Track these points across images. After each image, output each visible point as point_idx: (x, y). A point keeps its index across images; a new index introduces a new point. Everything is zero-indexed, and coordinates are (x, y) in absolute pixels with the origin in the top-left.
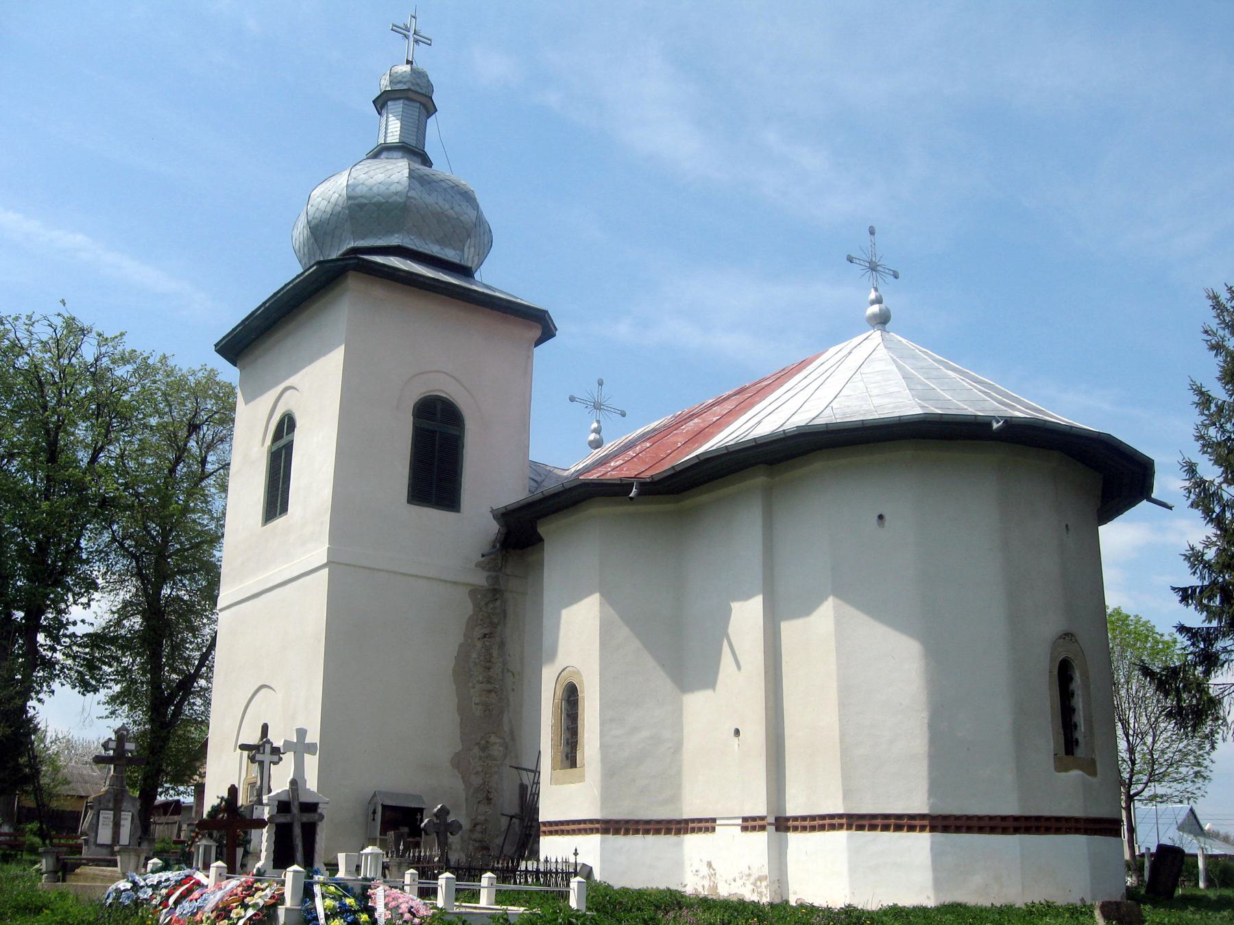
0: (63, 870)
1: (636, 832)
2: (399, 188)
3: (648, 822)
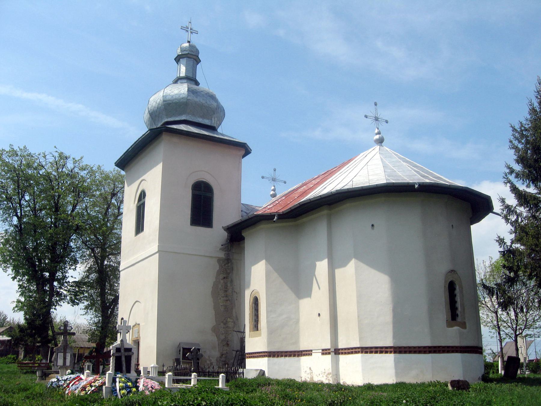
0: (45, 376)
1: (282, 356)
2: (184, 96)
3: (286, 352)
